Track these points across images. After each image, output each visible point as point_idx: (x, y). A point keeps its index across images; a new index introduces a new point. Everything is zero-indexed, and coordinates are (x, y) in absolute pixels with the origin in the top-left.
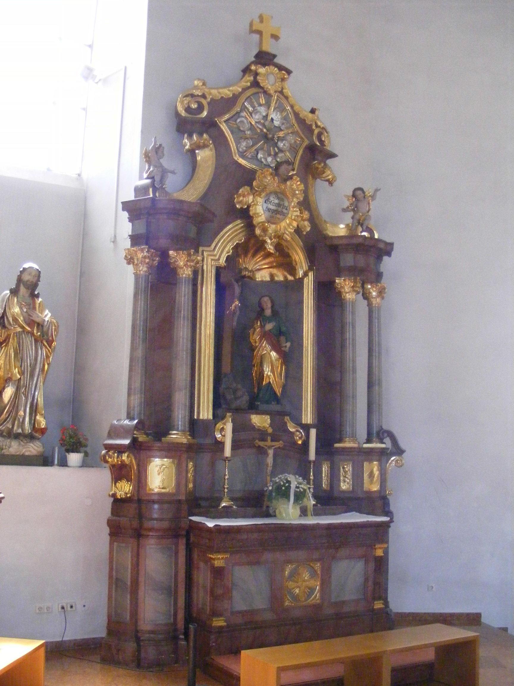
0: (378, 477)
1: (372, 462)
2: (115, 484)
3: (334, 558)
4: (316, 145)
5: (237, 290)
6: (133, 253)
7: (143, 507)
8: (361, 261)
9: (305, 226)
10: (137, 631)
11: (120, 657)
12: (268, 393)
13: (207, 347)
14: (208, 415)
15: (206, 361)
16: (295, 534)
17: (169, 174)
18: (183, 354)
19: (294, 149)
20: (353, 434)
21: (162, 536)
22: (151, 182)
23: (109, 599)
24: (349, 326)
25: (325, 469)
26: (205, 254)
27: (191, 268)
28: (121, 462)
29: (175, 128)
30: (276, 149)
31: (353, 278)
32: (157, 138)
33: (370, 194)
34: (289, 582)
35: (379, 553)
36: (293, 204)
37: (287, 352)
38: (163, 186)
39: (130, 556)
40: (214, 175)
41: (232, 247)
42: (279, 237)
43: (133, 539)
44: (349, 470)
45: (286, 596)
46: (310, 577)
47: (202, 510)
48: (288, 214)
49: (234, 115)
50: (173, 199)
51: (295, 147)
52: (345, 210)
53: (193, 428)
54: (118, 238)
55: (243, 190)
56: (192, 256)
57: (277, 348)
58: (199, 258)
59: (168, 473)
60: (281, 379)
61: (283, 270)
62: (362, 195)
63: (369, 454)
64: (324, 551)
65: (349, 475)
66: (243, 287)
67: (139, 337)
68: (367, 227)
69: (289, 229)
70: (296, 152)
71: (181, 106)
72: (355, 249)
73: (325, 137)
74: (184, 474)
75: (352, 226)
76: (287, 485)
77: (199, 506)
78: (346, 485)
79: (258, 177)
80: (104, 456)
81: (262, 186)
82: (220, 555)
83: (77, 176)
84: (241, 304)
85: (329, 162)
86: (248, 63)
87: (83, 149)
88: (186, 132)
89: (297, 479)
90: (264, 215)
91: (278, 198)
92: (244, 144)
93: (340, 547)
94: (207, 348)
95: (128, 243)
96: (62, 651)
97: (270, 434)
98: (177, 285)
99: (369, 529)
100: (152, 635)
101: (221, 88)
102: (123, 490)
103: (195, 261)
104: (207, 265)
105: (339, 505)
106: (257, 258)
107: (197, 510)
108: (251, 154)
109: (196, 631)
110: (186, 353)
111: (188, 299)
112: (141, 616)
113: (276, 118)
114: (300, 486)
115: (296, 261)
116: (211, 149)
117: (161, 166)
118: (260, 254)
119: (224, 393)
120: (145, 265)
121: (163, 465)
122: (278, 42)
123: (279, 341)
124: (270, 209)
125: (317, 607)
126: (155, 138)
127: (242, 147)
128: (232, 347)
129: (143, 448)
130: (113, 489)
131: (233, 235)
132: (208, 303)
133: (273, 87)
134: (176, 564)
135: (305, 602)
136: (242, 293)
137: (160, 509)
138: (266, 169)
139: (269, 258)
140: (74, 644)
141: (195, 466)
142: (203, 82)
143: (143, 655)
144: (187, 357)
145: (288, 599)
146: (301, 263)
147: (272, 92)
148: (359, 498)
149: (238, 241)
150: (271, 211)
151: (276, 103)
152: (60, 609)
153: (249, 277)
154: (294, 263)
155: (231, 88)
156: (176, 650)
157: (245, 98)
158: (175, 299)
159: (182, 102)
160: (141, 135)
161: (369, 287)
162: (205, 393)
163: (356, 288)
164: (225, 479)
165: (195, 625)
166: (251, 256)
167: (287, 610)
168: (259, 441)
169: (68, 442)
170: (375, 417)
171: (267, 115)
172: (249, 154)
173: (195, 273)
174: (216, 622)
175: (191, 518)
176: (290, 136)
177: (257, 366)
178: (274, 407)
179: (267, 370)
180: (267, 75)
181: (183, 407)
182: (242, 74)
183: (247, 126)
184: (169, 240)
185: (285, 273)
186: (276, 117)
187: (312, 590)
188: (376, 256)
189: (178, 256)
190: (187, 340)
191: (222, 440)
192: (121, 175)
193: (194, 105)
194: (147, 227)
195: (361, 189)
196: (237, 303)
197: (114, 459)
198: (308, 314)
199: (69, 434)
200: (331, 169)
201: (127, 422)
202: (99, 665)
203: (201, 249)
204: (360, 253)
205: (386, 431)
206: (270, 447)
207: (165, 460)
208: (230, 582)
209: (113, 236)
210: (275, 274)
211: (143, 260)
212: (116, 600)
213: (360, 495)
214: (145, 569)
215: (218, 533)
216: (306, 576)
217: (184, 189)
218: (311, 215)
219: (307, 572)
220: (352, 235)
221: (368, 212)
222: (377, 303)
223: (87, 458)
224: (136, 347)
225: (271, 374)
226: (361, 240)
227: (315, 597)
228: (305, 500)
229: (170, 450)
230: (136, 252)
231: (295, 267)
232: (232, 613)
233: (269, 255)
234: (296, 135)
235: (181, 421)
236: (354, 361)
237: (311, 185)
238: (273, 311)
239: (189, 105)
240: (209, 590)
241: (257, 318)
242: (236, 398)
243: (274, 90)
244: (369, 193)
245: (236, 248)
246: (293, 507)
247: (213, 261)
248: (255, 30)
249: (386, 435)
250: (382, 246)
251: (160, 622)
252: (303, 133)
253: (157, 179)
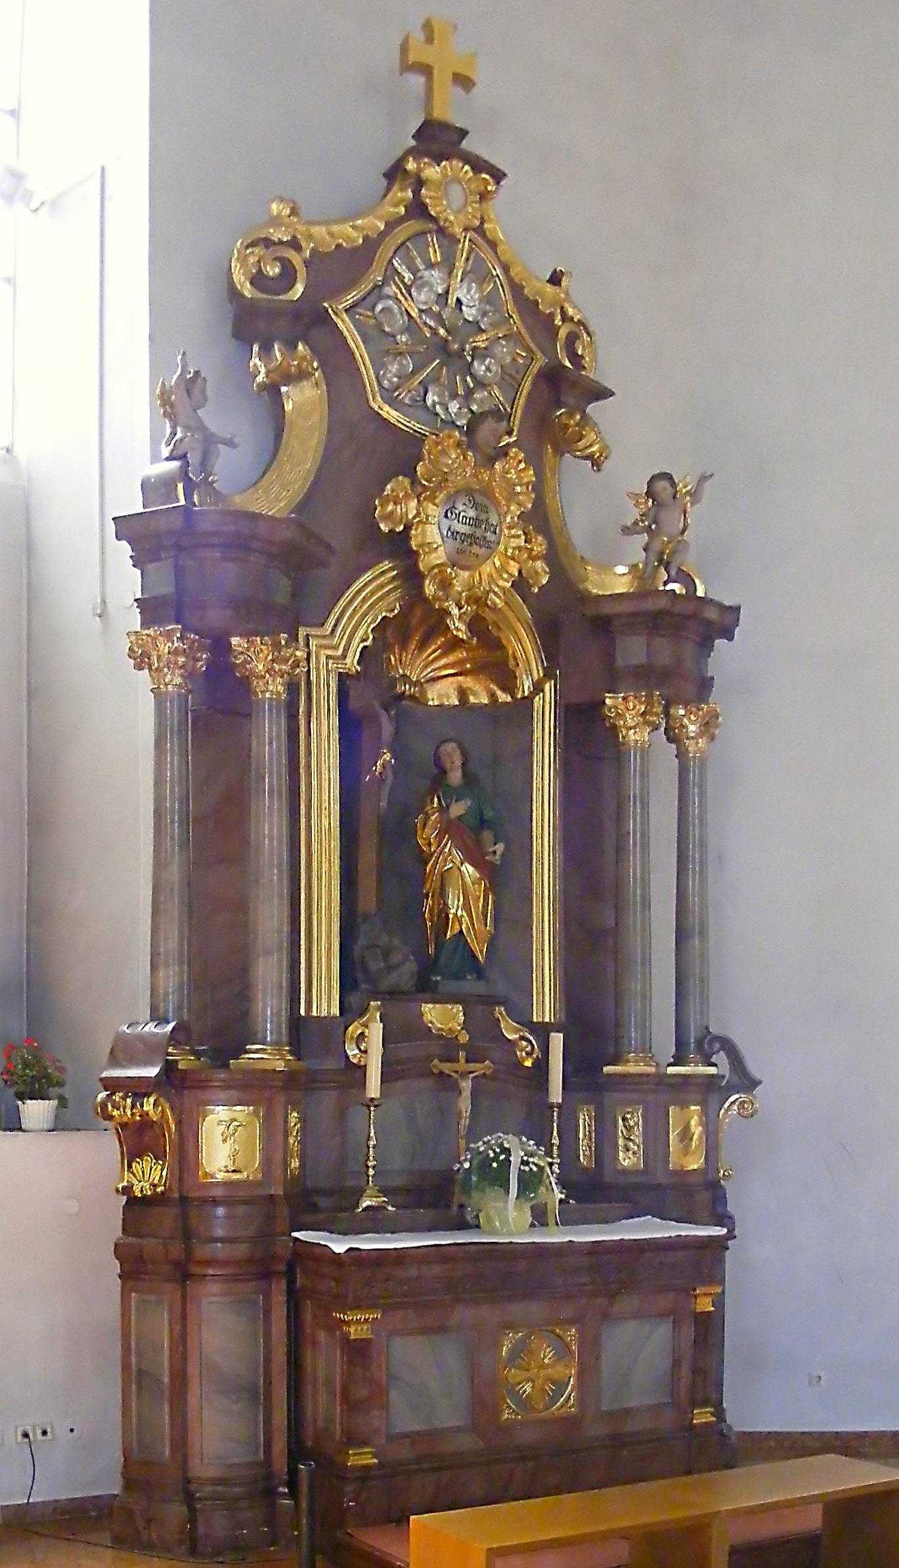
0: (700, 1138)
1: (688, 1107)
2: (130, 1166)
3: (605, 1316)
4: (565, 367)
5: (387, 728)
6: (147, 641)
7: (193, 1213)
8: (663, 651)
9: (537, 573)
10: (188, 1481)
11: (154, 1536)
12: (458, 956)
13: (324, 856)
14: (329, 1006)
15: (323, 888)
16: (522, 1266)
17: (220, 446)
18: (273, 875)
19: (510, 379)
20: (644, 1044)
21: (234, 1275)
22: (181, 467)
23: (123, 1370)
24: (635, 803)
25: (584, 1119)
26: (313, 643)
27: (282, 677)
28: (140, 1116)
29: (229, 328)
30: (468, 379)
31: (643, 694)
32: (189, 357)
33: (689, 487)
34: (510, 1370)
35: (705, 1305)
36: (508, 519)
37: (496, 865)
38: (208, 479)
39: (166, 1322)
40: (327, 448)
41: (372, 626)
42: (478, 601)
43: (172, 1285)
44: (637, 1124)
45: (504, 1399)
46: (555, 1358)
47: (321, 1216)
48: (498, 543)
49: (369, 293)
50: (234, 511)
51: (514, 373)
52: (627, 531)
53: (298, 1035)
54: (111, 607)
55: (397, 485)
56: (284, 649)
57: (475, 856)
58: (298, 653)
59: (244, 1137)
60: (486, 925)
61: (486, 680)
62: (670, 491)
63: (681, 1088)
64: (584, 1301)
65: (637, 1135)
66: (399, 721)
67: (172, 838)
68: (680, 570)
69: (501, 581)
70: (516, 386)
71: (242, 271)
72: (650, 625)
73: (584, 346)
74: (280, 1137)
75: (644, 570)
76: (502, 1157)
77: (314, 1208)
78: (630, 1158)
79: (429, 454)
80: (104, 1105)
81: (436, 477)
82: (370, 1314)
83: (4, 451)
84: (395, 760)
86: (399, 153)
87: (13, 384)
88: (255, 340)
89: (524, 1144)
90: (442, 548)
91: (475, 506)
92: (394, 368)
93: (619, 1292)
94: (324, 858)
95: (135, 619)
96: (30, 1524)
97: (464, 1047)
98: (254, 717)
99: (681, 1254)
100: (219, 1488)
101: (336, 222)
102: (146, 1178)
103: (291, 662)
104: (318, 669)
105: (616, 1202)
106: (429, 651)
107: (308, 1218)
108: (410, 395)
109: (312, 1475)
110: (278, 871)
111: (279, 749)
112: (194, 1448)
113: (468, 295)
114: (531, 1160)
115: (515, 658)
116: (316, 384)
117: (202, 427)
118: (436, 644)
119: (364, 958)
120: (177, 672)
121: (234, 1120)
122: (471, 95)
123: (479, 842)
124: (457, 533)
125: (570, 1423)
126: (184, 354)
127: (389, 375)
128: (379, 855)
129: (188, 1083)
130: (126, 1176)
131: (374, 598)
132: (323, 759)
133: (461, 217)
134: (268, 1335)
135: (544, 1411)
136: (397, 733)
137: (228, 1217)
138: (446, 432)
139: (455, 651)
140: (55, 1510)
141: (302, 1120)
142: (291, 205)
143: (201, 1529)
144: (280, 880)
145: (508, 1407)
146: (528, 661)
147: (457, 230)
148: (660, 1185)
149: (386, 611)
150: (458, 537)
151: (467, 259)
152: (20, 1437)
153: (412, 697)
154: (512, 662)
155: (359, 222)
156: (271, 1519)
157: (393, 248)
158: (250, 751)
159: (243, 260)
160: (150, 347)
161: (682, 712)
162: (323, 959)
163: (651, 716)
164: (369, 1147)
165: (311, 1465)
166: (415, 648)
167: (509, 1427)
168: (441, 1061)
169: (22, 1076)
170: (693, 1008)
171: (447, 292)
172: (406, 395)
173: (292, 688)
174: (356, 1458)
175: (295, 1234)
176: (503, 346)
177: (433, 896)
178: (471, 985)
179: (455, 905)
180: (444, 184)
181: (275, 991)
182: (384, 182)
183: (402, 321)
184: (229, 612)
185: (492, 686)
186: (468, 297)
187: (561, 1386)
188: (698, 639)
189: (253, 649)
190: (280, 841)
191: (360, 1060)
192: (107, 451)
193: (273, 268)
194: (176, 580)
195: (668, 477)
196: (387, 757)
197: (124, 1112)
198: (542, 780)
199: (22, 1058)
200: (598, 428)
201: (151, 1028)
202: (109, 1551)
203: (302, 632)
204: (662, 632)
205: (718, 1037)
206: (464, 1075)
207: (239, 1108)
208: (384, 1372)
209: (99, 600)
210: (469, 688)
211: (172, 658)
212: (139, 1416)
213: (662, 1179)
214: (201, 1348)
215: (354, 1266)
216: (547, 1355)
217: (258, 485)
218: (551, 545)
219: (549, 1347)
220: (645, 591)
221: (683, 532)
222: (699, 749)
223: (65, 1109)
224: (166, 859)
225: (465, 914)
226: (663, 603)
227: (567, 1402)
228: (542, 1189)
229: (248, 1086)
230: (154, 639)
231: (514, 672)
232: (391, 1438)
233: (455, 643)
234: (515, 343)
235: (271, 1023)
236: (645, 883)
237: (550, 471)
238: (464, 774)
239: (260, 267)
240: (338, 1390)
241: (432, 792)
242: (390, 968)
243: (462, 225)
244: (686, 487)
245: (381, 628)
246: (515, 1207)
247: (331, 661)
248: (413, 64)
249: (717, 1046)
250: (712, 614)
251: (236, 1461)
252: (532, 338)
253: (194, 458)
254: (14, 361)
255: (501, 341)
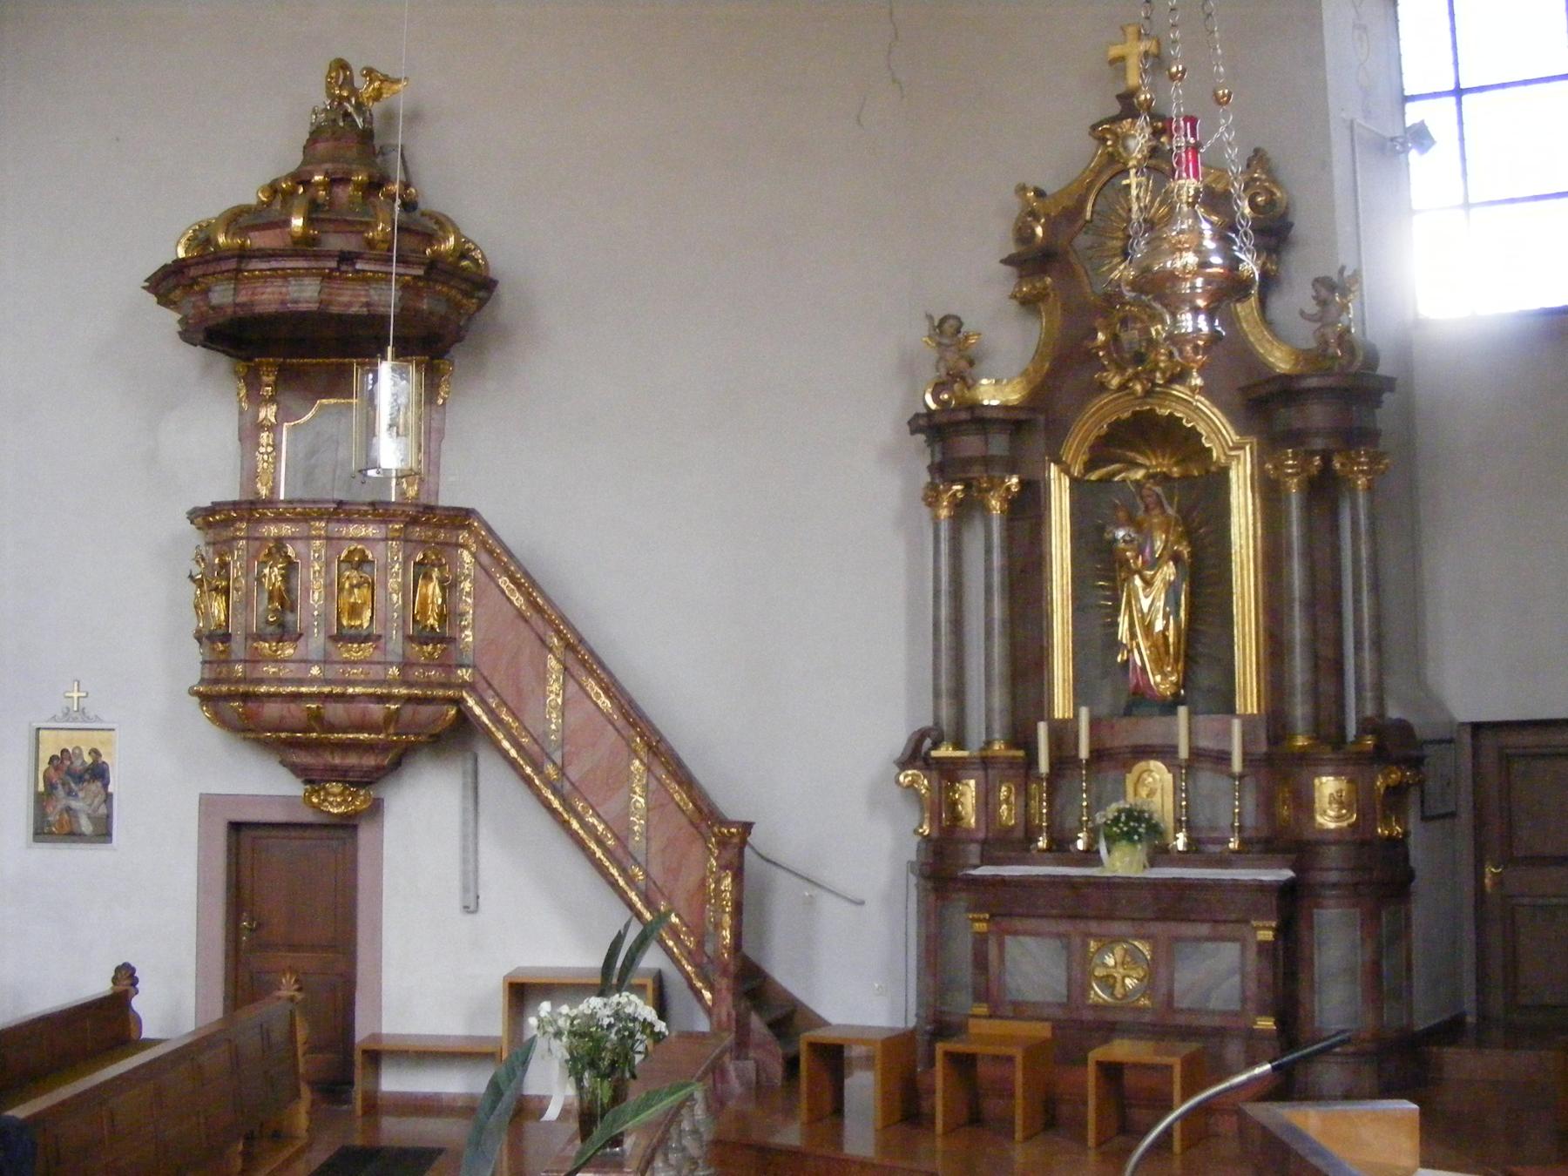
85: (1012, 249)
134: (504, 754)
158: (1022, 916)
163: (401, 528)
232: (1242, 941)
254: (1461, 122)
255: (696, 1173)
